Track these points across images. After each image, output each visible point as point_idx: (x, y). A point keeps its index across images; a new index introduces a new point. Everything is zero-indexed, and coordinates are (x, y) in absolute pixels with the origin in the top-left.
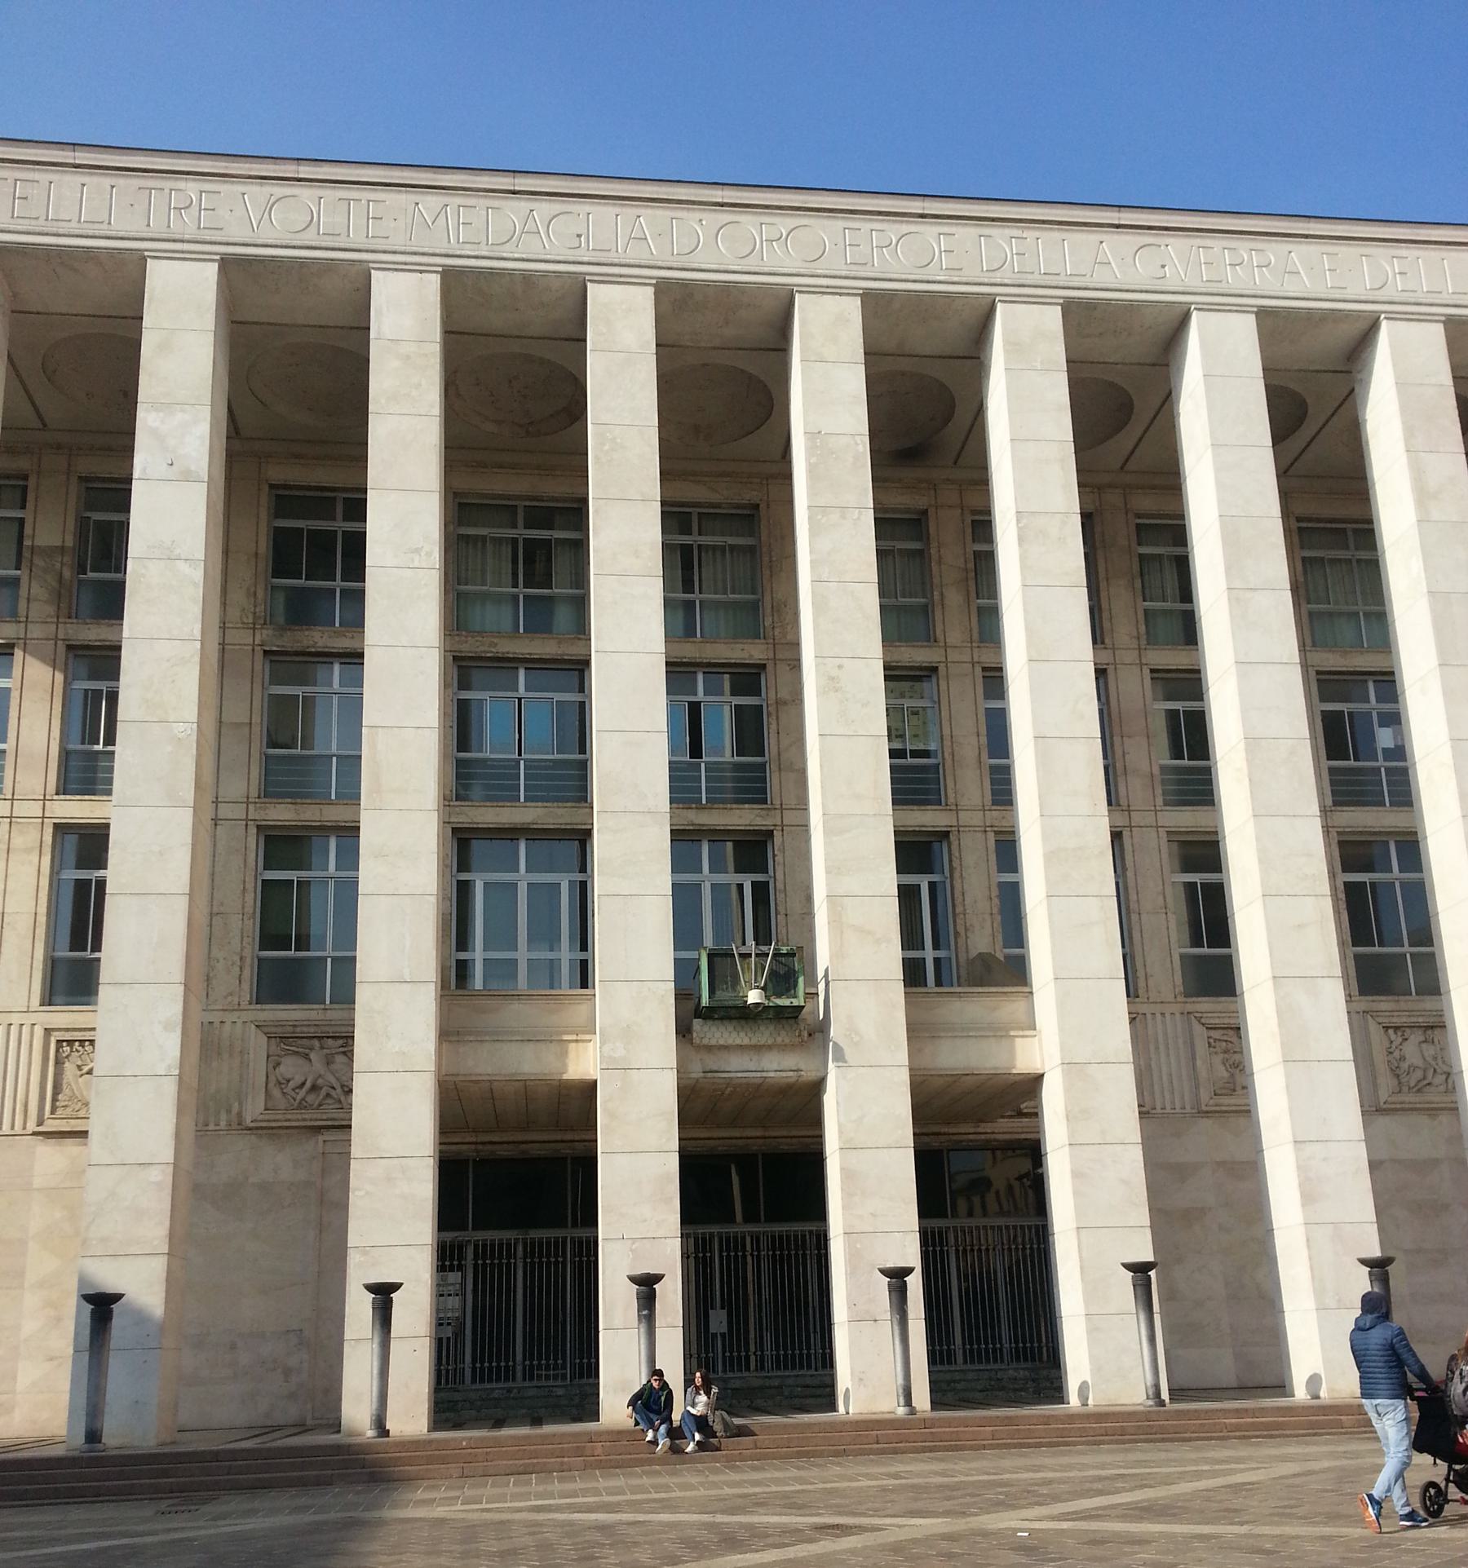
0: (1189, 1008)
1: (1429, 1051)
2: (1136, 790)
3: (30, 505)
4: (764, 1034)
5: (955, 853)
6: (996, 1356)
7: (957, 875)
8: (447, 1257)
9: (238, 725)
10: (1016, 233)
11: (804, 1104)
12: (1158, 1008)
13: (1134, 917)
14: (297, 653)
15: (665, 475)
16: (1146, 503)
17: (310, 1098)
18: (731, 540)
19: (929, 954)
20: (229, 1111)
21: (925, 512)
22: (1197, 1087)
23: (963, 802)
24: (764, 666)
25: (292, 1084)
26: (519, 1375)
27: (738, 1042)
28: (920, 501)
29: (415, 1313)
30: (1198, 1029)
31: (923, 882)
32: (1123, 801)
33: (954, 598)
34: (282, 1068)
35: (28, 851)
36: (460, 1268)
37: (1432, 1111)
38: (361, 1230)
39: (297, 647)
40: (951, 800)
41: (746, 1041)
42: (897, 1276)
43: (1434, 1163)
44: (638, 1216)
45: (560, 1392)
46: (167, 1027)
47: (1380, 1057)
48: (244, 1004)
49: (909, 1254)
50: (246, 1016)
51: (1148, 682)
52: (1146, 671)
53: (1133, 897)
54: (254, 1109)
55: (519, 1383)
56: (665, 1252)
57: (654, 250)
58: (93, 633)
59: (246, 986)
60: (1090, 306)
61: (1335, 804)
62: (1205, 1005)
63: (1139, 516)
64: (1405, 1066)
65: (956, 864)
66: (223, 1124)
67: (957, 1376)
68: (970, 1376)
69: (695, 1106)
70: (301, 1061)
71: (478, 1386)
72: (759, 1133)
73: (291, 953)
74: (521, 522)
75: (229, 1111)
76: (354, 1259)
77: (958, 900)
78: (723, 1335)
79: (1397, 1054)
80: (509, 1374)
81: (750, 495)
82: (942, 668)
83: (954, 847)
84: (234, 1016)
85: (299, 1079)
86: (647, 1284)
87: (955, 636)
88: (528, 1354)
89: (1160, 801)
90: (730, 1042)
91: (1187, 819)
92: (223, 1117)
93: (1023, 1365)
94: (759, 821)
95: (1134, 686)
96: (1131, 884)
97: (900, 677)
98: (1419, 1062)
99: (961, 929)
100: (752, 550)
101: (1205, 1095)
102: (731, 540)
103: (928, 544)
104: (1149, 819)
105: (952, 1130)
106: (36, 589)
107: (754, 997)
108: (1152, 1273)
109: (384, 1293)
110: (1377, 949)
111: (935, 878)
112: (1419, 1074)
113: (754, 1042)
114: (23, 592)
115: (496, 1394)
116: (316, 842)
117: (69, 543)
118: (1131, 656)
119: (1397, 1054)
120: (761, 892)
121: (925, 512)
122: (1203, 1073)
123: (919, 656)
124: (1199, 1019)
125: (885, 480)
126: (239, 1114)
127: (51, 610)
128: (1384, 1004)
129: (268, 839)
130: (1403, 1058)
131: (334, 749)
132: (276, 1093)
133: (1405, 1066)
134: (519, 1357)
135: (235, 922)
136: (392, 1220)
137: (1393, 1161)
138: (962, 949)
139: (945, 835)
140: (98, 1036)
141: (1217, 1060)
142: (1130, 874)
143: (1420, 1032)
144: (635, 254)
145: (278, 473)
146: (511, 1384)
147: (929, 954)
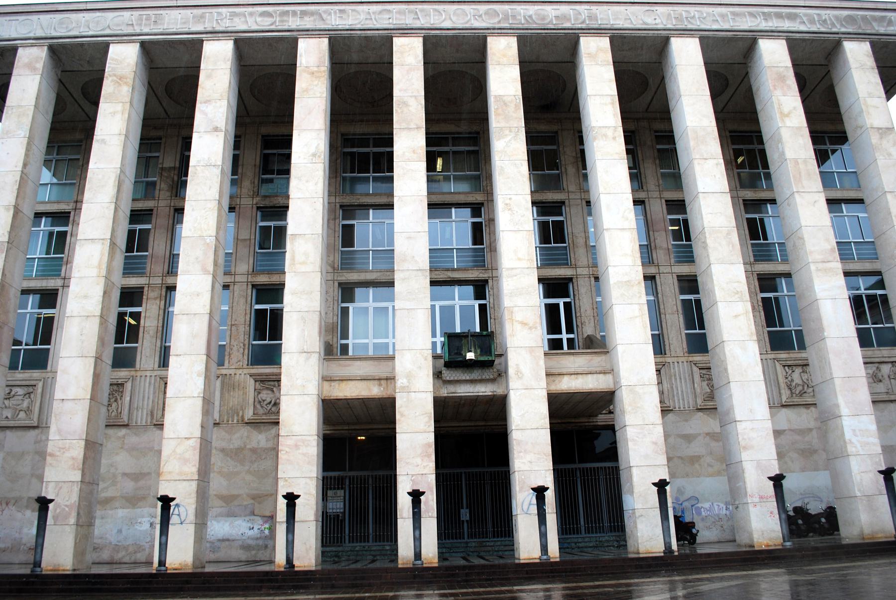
0: (691, 359)
1: (805, 377)
2: (660, 256)
3: (242, 148)
4: (476, 374)
5: (576, 288)
6: (601, 530)
7: (577, 298)
8: (327, 485)
9: (245, 240)
10: (588, 7)
11: (498, 408)
12: (675, 360)
13: (662, 316)
14: (271, 207)
15: (428, 121)
16: (658, 126)
17: (273, 409)
18: (467, 148)
19: (564, 336)
20: (238, 415)
21: (556, 132)
22: (696, 397)
23: (579, 264)
24: (482, 204)
25: (266, 403)
26: (466, 536)
27: (464, 378)
28: (555, 128)
29: (308, 510)
30: (695, 369)
31: (561, 302)
32: (655, 262)
33: (571, 170)
34: (261, 395)
35: (155, 299)
36: (342, 488)
37: (807, 406)
38: (284, 471)
39: (271, 204)
40: (573, 263)
41: (468, 378)
42: (540, 491)
43: (811, 430)
44: (415, 461)
45: (388, 548)
46: (199, 375)
47: (781, 380)
48: (245, 366)
49: (547, 479)
50: (246, 371)
51: (664, 206)
52: (663, 201)
53: (662, 307)
54: (249, 414)
55: (370, 544)
56: (428, 482)
57: (423, 22)
58: (673, 195)
59: (246, 357)
60: (623, 37)
61: (755, 260)
62: (698, 358)
63: (656, 132)
64: (794, 384)
65: (576, 293)
66: (235, 421)
67: (580, 540)
68: (586, 540)
69: (444, 410)
70: (269, 392)
71: (351, 545)
72: (483, 423)
73: (266, 342)
74: (371, 145)
75: (238, 415)
76: (281, 483)
77: (578, 310)
78: (467, 521)
79: (790, 378)
80: (461, 537)
81: (475, 128)
82: (567, 202)
83: (575, 284)
84: (240, 371)
85: (268, 400)
86: (540, 491)
87: (572, 188)
88: (587, 521)
89: (673, 260)
90: (460, 378)
91: (685, 269)
92: (236, 418)
93: (614, 534)
94: (481, 275)
95: (658, 208)
96: (660, 301)
97: (542, 207)
98: (800, 382)
99: (580, 325)
100: (476, 153)
101: (699, 401)
102: (467, 148)
103: (558, 146)
104: (668, 269)
105: (577, 421)
106: (163, 185)
107: (470, 356)
108: (668, 488)
109: (291, 499)
110: (778, 329)
111: (567, 300)
112: (800, 388)
113: (472, 378)
114: (158, 187)
115: (357, 549)
116: (778, 280)
117: (177, 165)
118: (656, 194)
119: (790, 378)
120: (483, 309)
121: (556, 132)
122: (698, 390)
123: (551, 196)
124: (695, 364)
125: (628, 119)
126: (243, 416)
127: (168, 194)
128: (783, 355)
129: (258, 291)
130: (792, 380)
131: (371, 248)
132: (258, 406)
133: (794, 384)
134: (347, 532)
135: (242, 329)
136: (300, 465)
137: (790, 430)
138: (580, 333)
139: (571, 279)
140: (810, 363)
141: (705, 384)
142: (660, 296)
143: (800, 368)
144: (417, 24)
145: (264, 130)
146: (366, 544)
147: (564, 336)
